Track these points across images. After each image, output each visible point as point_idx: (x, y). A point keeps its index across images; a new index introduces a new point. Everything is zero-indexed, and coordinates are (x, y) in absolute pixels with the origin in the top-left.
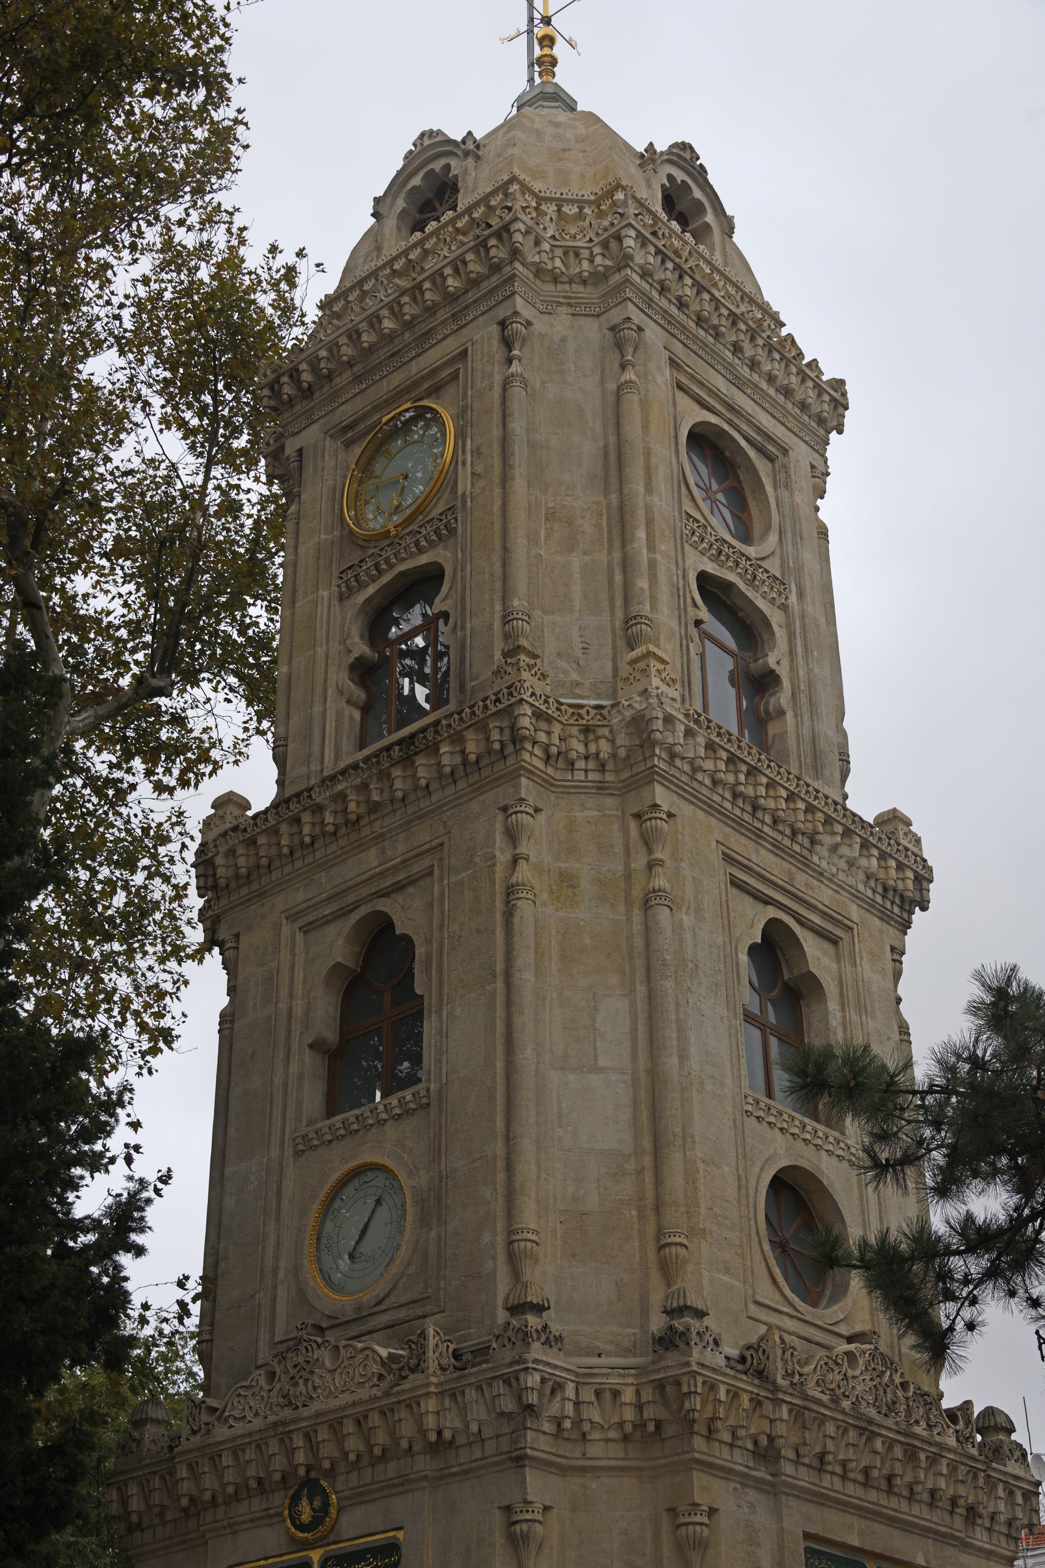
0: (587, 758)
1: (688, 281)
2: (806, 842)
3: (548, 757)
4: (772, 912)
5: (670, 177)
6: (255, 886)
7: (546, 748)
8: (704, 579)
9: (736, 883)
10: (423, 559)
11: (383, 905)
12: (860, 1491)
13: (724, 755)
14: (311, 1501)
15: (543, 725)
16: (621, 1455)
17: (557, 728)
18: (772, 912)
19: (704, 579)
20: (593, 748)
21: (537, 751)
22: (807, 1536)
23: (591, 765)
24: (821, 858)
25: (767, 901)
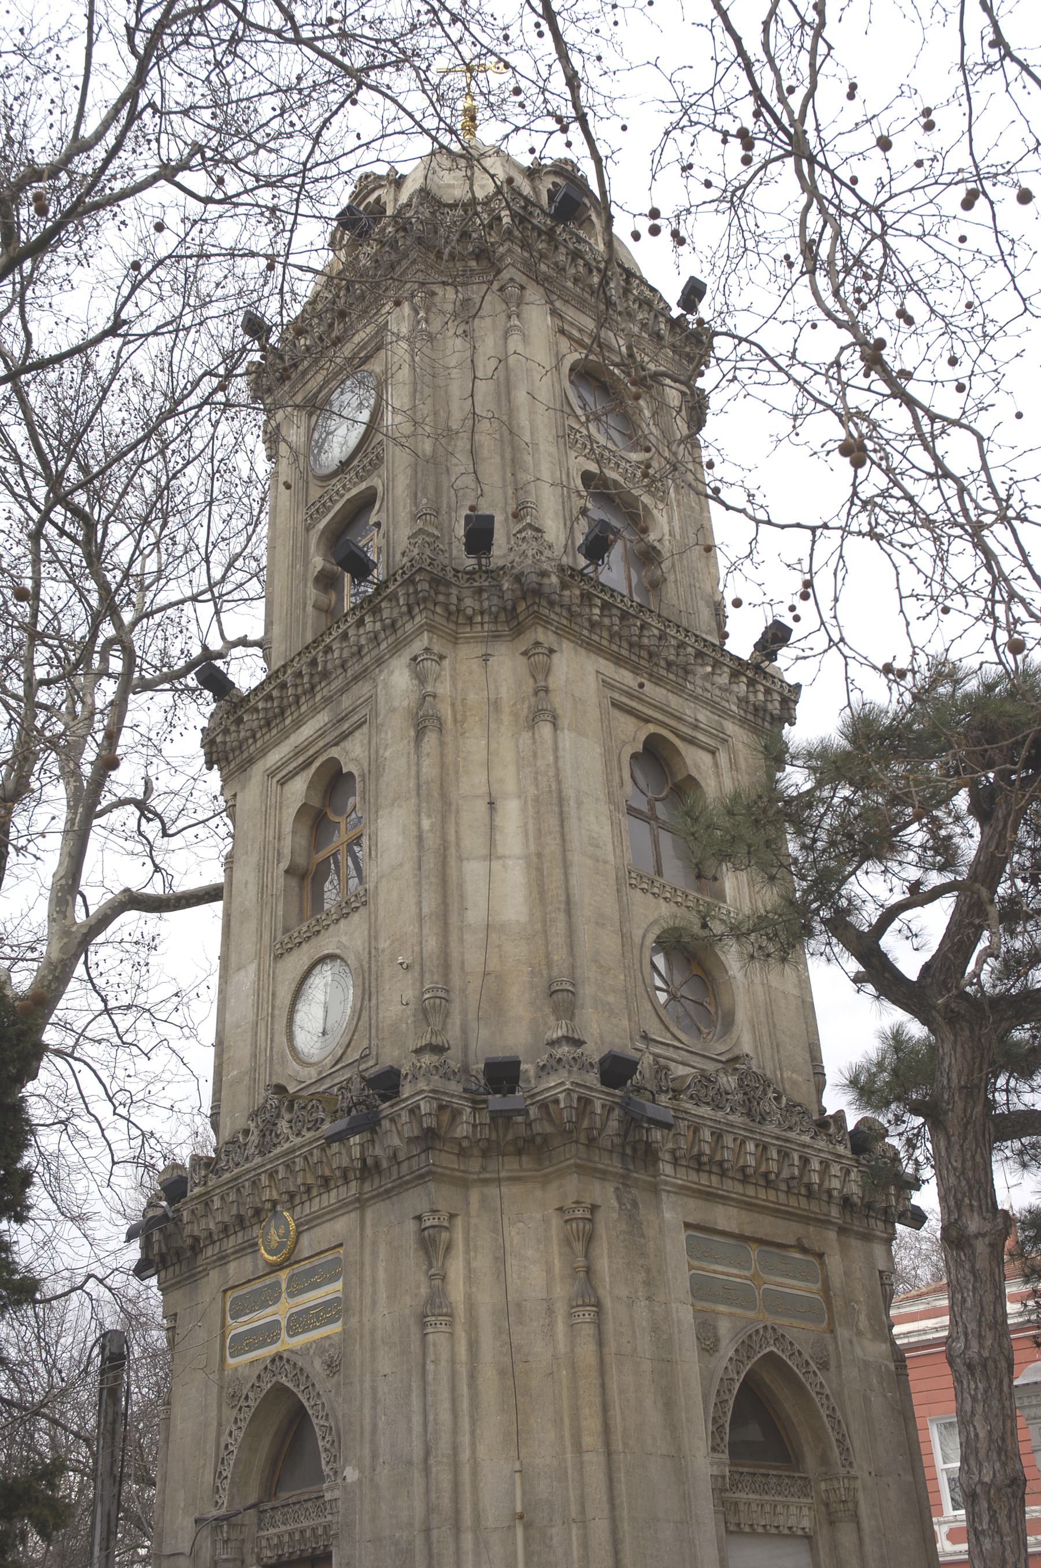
0: (482, 613)
1: (562, 250)
2: (681, 673)
3: (450, 613)
4: (652, 728)
5: (554, 184)
6: (245, 755)
7: (446, 606)
8: (587, 477)
9: (616, 705)
10: (363, 486)
11: (334, 752)
12: (739, 1188)
13: (599, 602)
14: (277, 1228)
15: (442, 589)
16: (516, 1166)
17: (454, 591)
18: (652, 728)
19: (587, 477)
20: (486, 604)
21: (438, 610)
22: (688, 1225)
23: (486, 619)
24: (697, 684)
25: (647, 720)
